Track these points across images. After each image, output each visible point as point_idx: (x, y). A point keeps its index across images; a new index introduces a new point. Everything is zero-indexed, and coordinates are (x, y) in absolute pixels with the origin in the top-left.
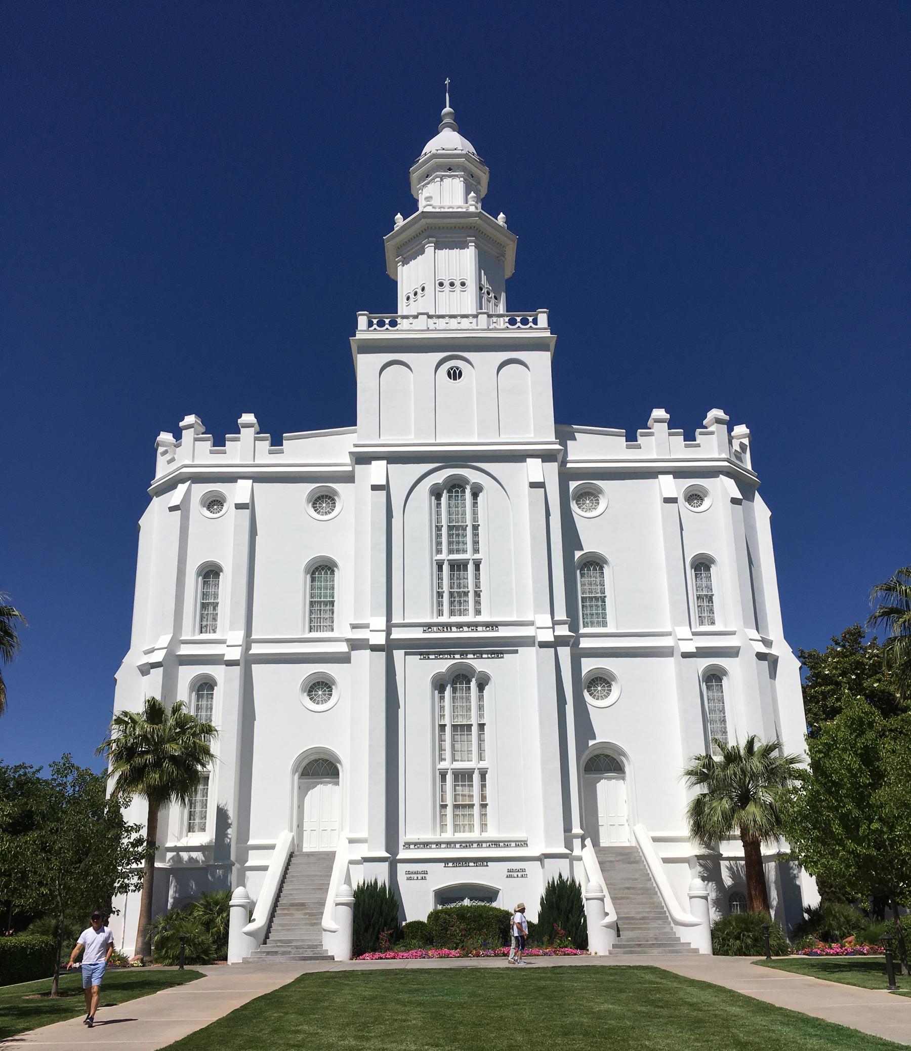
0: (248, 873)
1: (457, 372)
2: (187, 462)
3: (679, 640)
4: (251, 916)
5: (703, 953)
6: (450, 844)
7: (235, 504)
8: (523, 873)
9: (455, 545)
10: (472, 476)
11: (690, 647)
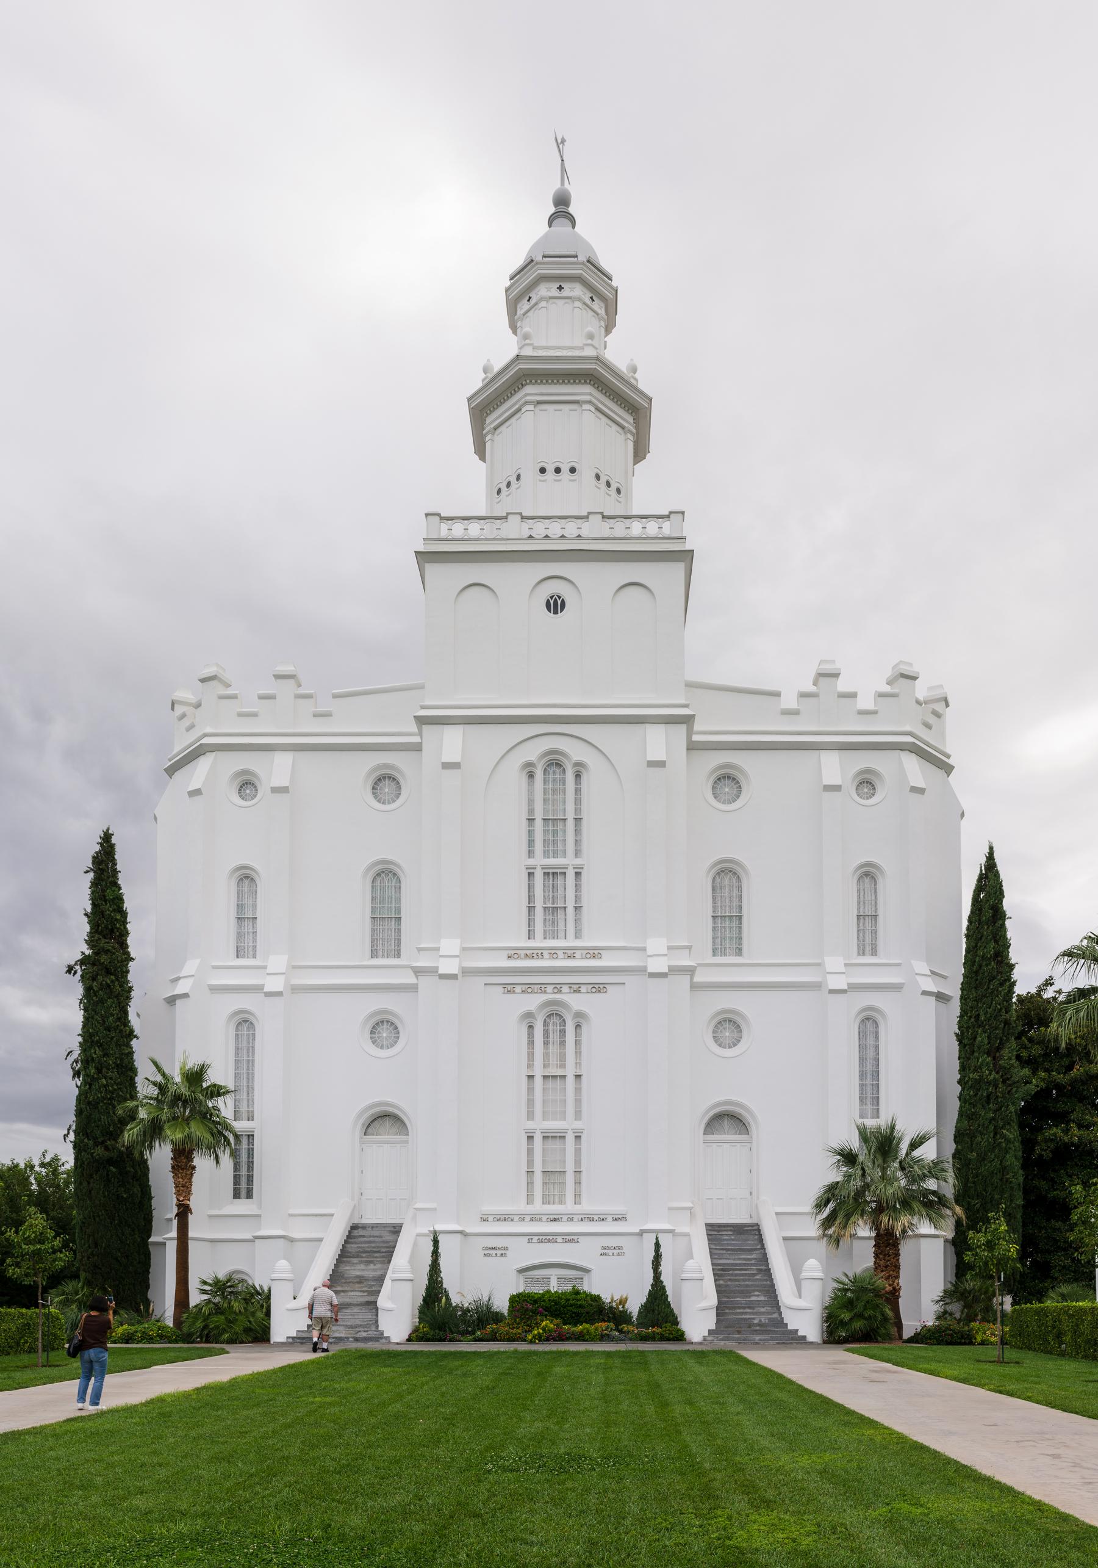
0: (803, 1282)
1: (559, 602)
2: (209, 730)
3: (844, 973)
4: (615, 1316)
5: (811, 1341)
6: (535, 1218)
7: (288, 792)
8: (619, 1251)
9: (553, 846)
10: (575, 752)
11: (840, 983)
